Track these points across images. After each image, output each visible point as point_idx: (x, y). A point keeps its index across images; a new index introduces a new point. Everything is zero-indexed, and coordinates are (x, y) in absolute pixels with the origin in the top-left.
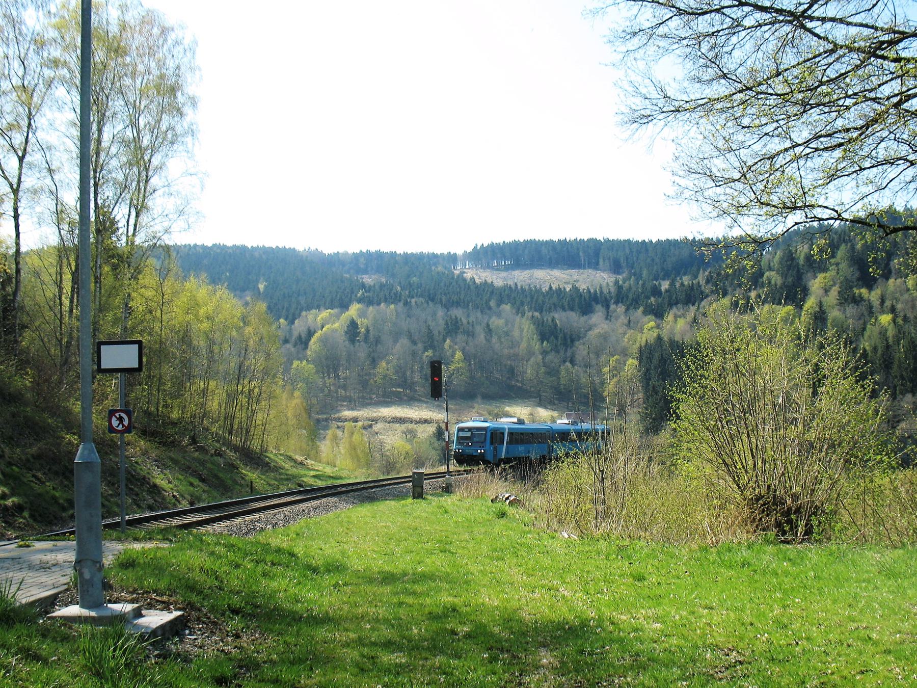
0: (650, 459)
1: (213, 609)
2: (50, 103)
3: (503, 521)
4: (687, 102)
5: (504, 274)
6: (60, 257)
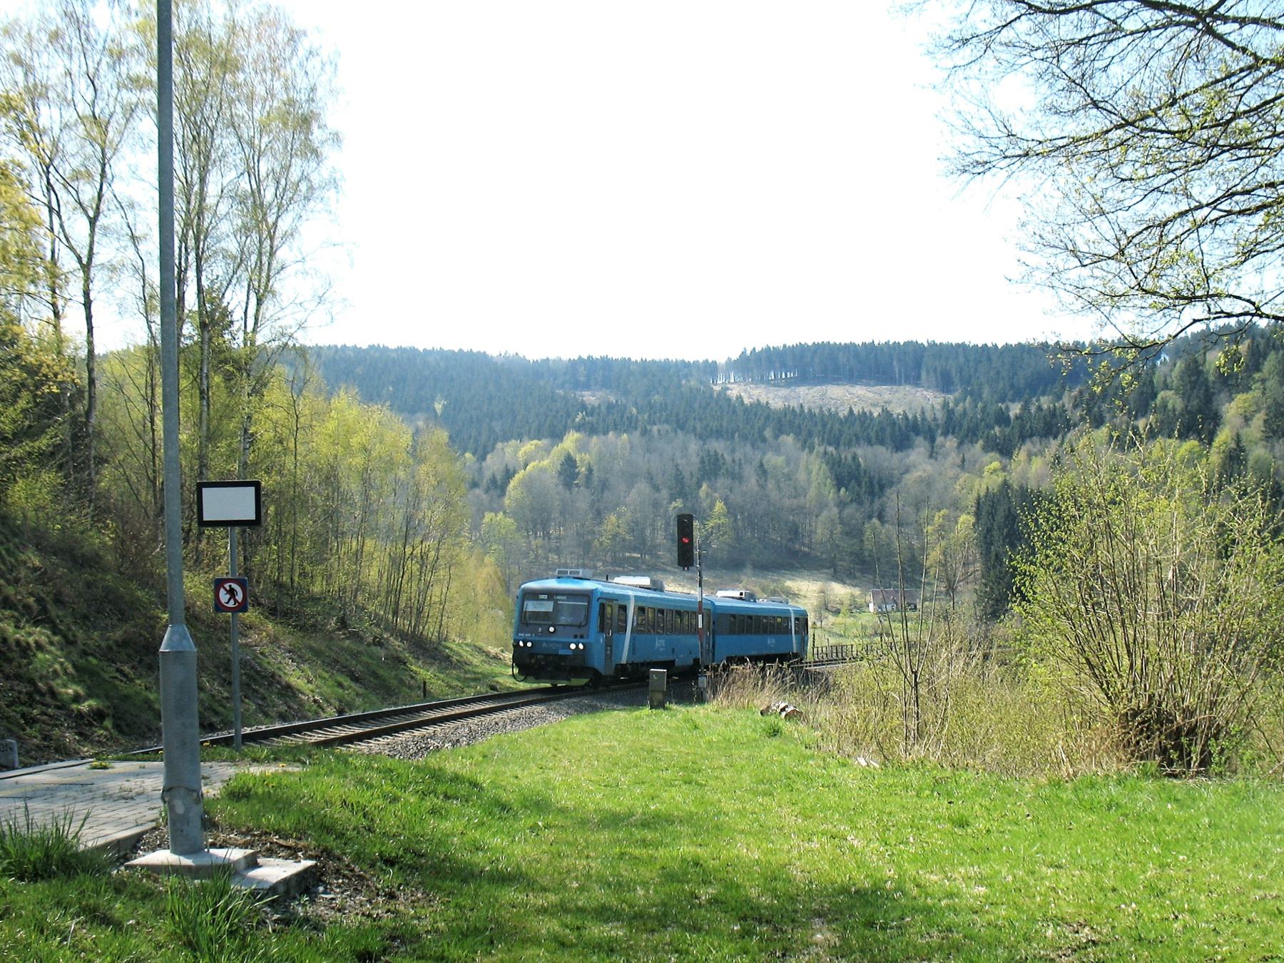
0: (986, 657)
1: (358, 857)
2: (131, 141)
3: (775, 742)
4: (1040, 142)
5: (784, 392)
6: (151, 361)
